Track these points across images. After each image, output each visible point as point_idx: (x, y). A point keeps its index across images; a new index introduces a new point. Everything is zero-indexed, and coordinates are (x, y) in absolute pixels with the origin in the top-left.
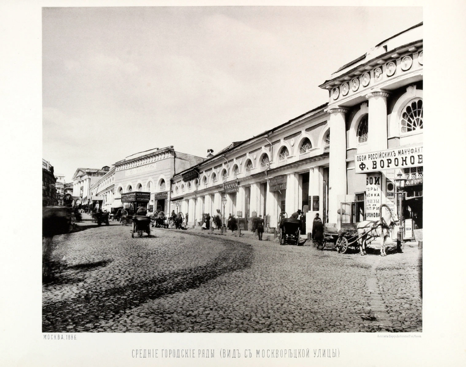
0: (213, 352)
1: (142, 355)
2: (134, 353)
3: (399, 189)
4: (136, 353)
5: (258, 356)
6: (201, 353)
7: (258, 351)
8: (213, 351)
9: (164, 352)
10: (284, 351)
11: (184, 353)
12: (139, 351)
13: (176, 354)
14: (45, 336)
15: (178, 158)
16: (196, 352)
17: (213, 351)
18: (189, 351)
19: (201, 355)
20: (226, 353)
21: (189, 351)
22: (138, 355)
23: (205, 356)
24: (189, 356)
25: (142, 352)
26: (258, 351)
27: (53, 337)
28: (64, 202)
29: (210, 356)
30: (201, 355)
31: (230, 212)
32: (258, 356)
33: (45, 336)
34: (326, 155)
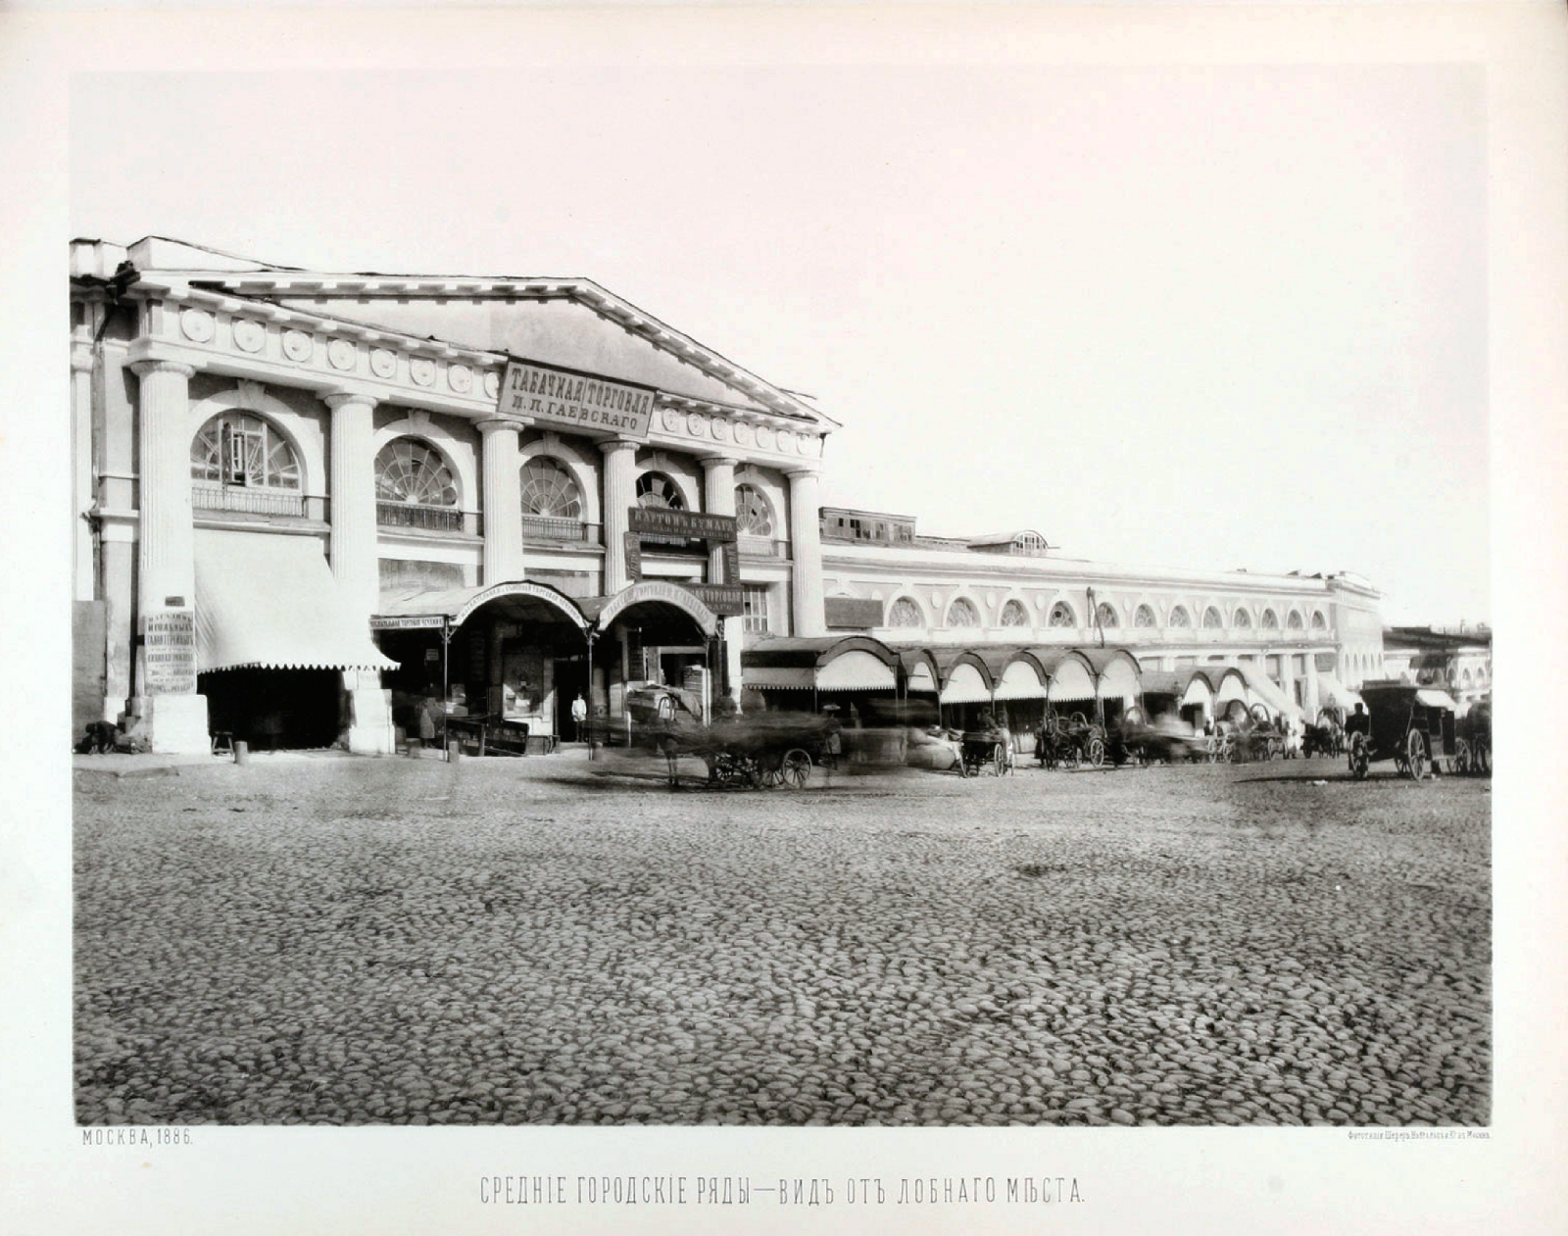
0: (744, 1188)
1: (514, 1196)
2: (489, 1188)
3: (1474, 764)
4: (493, 1189)
5: (87, 1142)
6: (709, 1188)
7: (1013, 1182)
8: (744, 1181)
9: (585, 1184)
10: (599, 1181)
11: (650, 1189)
12: (504, 1180)
13: (625, 1192)
14: (87, 1136)
15: (175, 370)
16: (691, 1187)
17: (744, 1181)
18: (667, 1182)
19: (705, 1196)
20: (790, 1191)
21: (667, 1182)
22: (501, 1197)
23: (720, 1199)
24: (667, 1198)
25: (514, 1184)
26: (1013, 1182)
27: (114, 1136)
28: (633, 718)
29: (736, 1200)
30: (705, 1196)
31: (74, 589)
32: (1013, 1198)
33: (87, 1136)
34: (1490, 685)
